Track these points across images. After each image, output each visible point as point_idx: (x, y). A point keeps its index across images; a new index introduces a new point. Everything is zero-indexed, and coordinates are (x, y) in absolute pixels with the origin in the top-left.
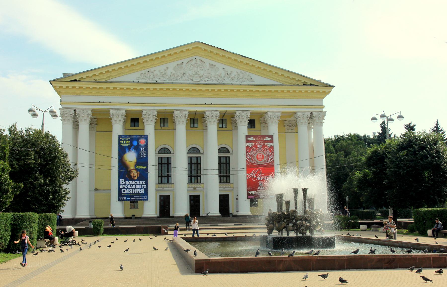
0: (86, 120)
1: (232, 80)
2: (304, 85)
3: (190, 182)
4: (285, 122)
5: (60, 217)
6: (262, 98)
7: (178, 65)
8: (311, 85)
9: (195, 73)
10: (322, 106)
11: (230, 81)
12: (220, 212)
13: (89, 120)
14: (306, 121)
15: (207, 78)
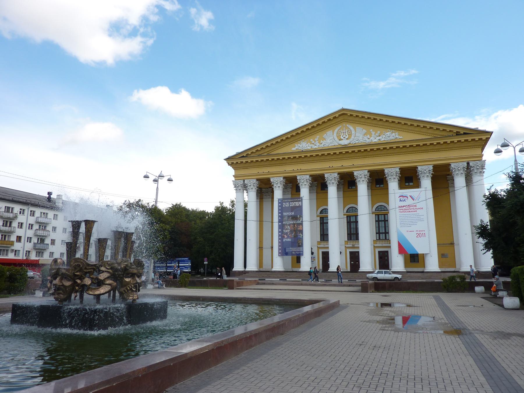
0: (252, 188)
2: (457, 135)
3: (17, 251)
4: (448, 176)
5: (101, 271)
8: (465, 134)
13: (431, 176)
14: (462, 172)
15: (354, 141)
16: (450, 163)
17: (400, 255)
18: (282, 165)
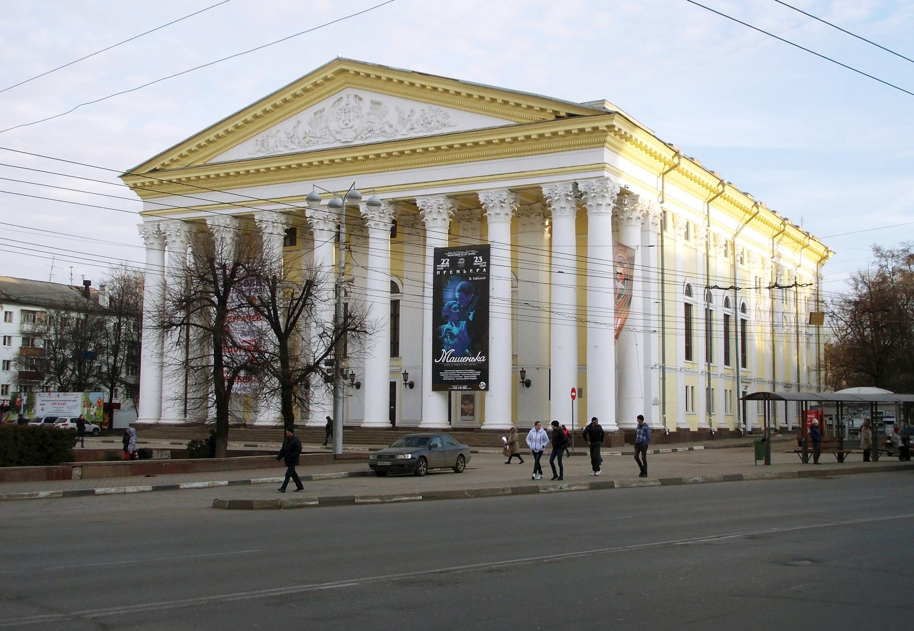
1: (412, 129)
6: (538, 153)
7: (315, 113)
8: (570, 116)
9: (344, 125)
10: (601, 165)
11: (408, 132)
12: (390, 420)
15: (365, 133)
16: (541, 185)
17: (434, 393)
18: (547, 153)
